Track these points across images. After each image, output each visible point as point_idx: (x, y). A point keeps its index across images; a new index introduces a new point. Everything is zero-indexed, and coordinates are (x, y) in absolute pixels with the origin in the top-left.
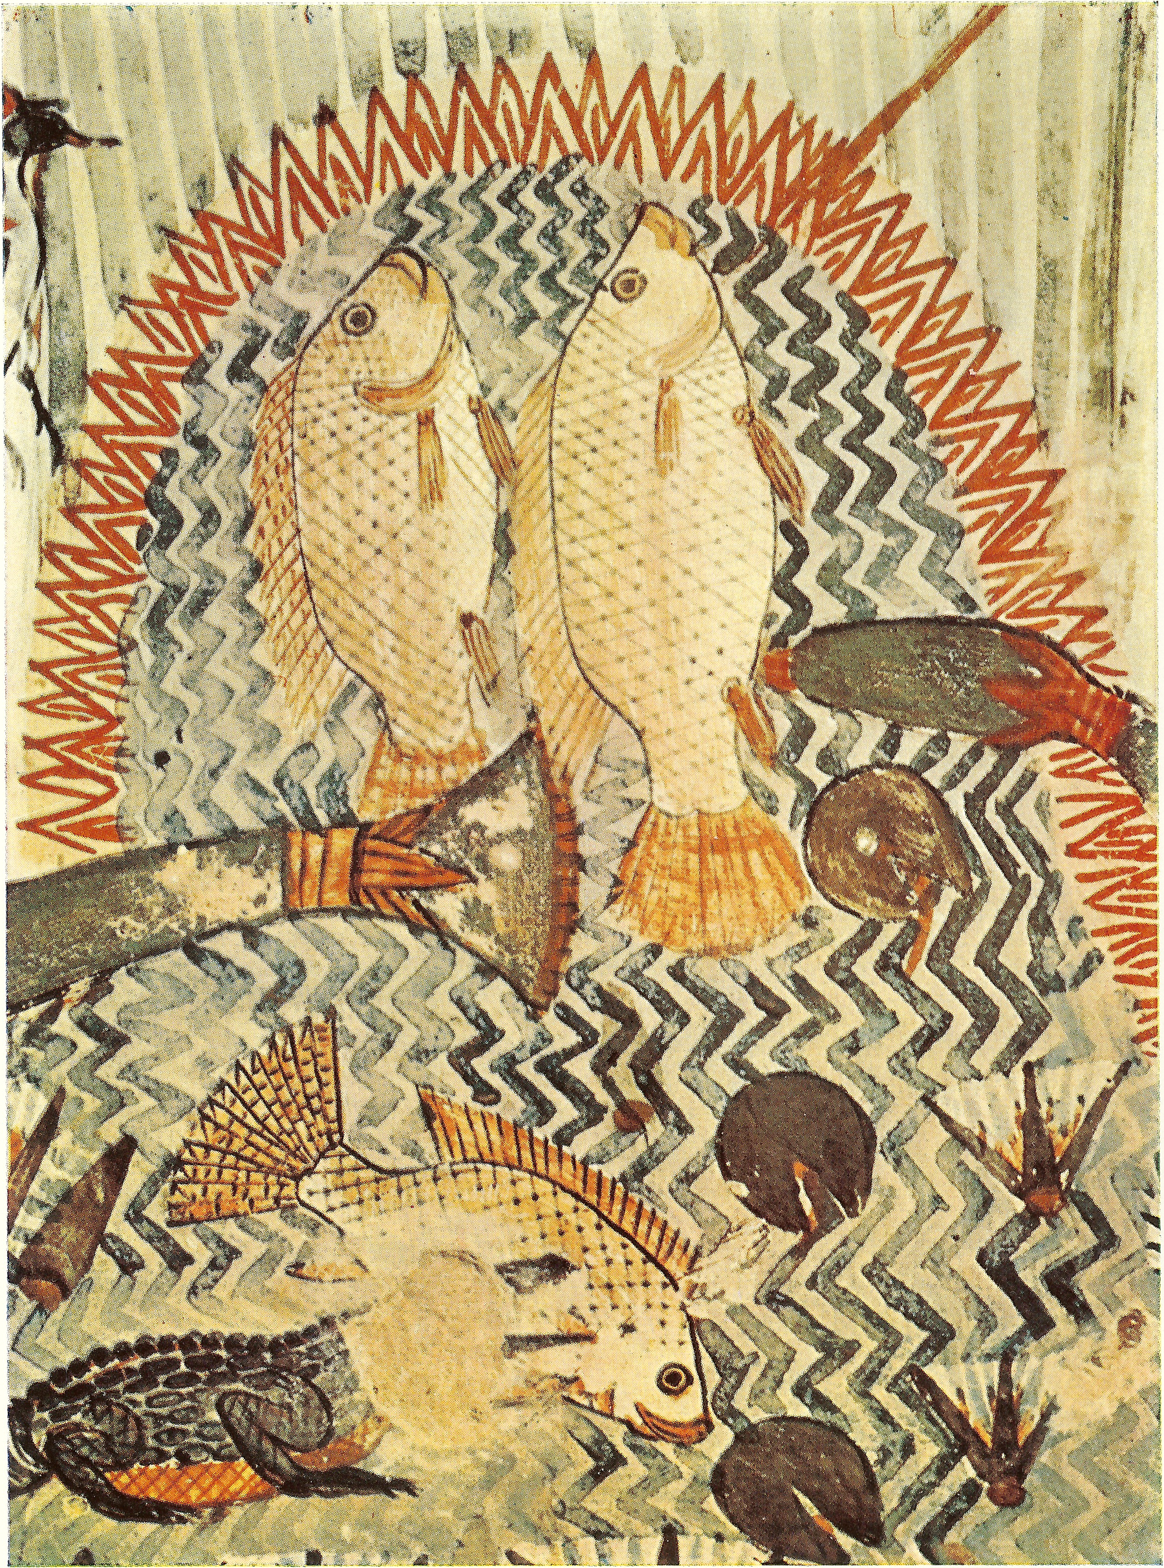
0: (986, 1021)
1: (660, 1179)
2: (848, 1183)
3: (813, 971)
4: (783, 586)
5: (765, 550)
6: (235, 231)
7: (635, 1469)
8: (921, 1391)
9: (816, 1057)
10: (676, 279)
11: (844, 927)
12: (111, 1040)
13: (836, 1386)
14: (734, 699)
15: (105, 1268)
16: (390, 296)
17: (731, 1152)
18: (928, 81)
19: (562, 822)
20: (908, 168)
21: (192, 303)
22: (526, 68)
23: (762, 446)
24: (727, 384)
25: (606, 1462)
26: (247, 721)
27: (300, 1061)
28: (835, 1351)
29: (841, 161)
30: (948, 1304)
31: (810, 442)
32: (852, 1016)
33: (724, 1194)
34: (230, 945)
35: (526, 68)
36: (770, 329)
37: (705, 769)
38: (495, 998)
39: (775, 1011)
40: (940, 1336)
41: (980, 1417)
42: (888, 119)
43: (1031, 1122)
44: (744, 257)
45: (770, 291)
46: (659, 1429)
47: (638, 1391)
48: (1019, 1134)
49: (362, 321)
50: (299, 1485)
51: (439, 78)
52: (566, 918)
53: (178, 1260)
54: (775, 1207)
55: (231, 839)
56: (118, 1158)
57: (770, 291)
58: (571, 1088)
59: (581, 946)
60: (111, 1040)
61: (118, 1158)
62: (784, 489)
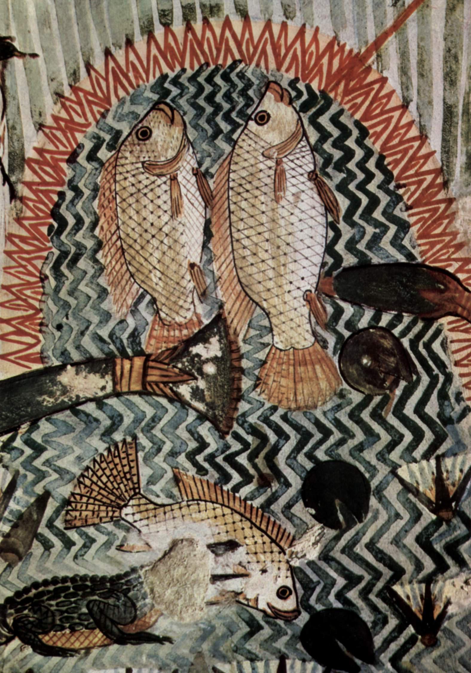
0: (418, 436)
1: (277, 507)
2: (358, 510)
3: (343, 417)
4: (330, 249)
7: (267, 631)
9: (344, 452)
11: (356, 397)
12: (39, 449)
14: (307, 298)
15: (37, 548)
17: (307, 495)
23: (321, 189)
28: (353, 580)
31: (342, 188)
34: (90, 408)
36: (324, 135)
39: (326, 433)
40: (398, 573)
44: (313, 105)
45: (324, 120)
46: (277, 613)
49: (145, 134)
50: (122, 639)
53: (68, 544)
54: (325, 517)
56: (42, 501)
57: (324, 120)
61: (42, 501)
62: (330, 207)
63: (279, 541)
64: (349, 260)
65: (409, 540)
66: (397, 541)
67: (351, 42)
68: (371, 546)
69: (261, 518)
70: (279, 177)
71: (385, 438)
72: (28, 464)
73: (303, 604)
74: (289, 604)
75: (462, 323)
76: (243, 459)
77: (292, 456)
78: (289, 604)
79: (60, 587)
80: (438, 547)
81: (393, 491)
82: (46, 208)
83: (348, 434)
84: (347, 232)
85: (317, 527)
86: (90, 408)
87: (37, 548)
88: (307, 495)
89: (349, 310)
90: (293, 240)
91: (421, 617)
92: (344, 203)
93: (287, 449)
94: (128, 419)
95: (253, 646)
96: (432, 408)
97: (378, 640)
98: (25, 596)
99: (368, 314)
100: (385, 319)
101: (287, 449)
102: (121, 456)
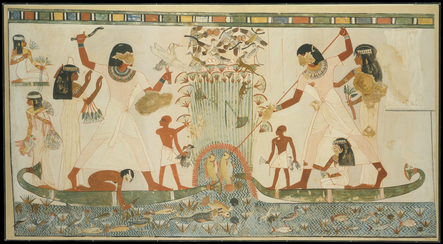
0: (245, 195)
1: (227, 204)
2: (237, 204)
3: (235, 192)
4: (233, 171)
5: (232, 170)
6: (203, 153)
7: (226, 219)
8: (241, 214)
9: (235, 197)
10: (228, 156)
11: (237, 190)
12: (197, 197)
13: (236, 215)
14: (231, 178)
15: (197, 209)
16: (212, 156)
17: (231, 202)
18: (247, 137)
19: (221, 185)
20: (240, 149)
21: (201, 157)
22: (219, 144)
23: (232, 164)
24: (230, 161)
25: (224, 219)
26: (203, 180)
27: (207, 197)
28: (236, 213)
29: (236, 148)
30: (242, 210)
31: (235, 164)
32: (237, 195)
33: (230, 204)
34: (204, 192)
35: (219, 144)
36: (232, 157)
37: (229, 182)
38: (218, 194)
39: (233, 195)
40: (242, 212)
41: (244, 216)
42: (239, 146)
43: (247, 200)
44: (231, 154)
45: (232, 156)
46: (227, 217)
47: (226, 215)
48: (413, 168)
49: (210, 157)
50: (208, 220)
51: (214, 144)
52: (222, 190)
53: (201, 208)
54: (233, 205)
55: (203, 186)
56: (197, 203)
57: (232, 156)
58: (221, 199)
59: (222, 192)
60: (197, 197)
61: (197, 203)
62: (233, 166)
63: (228, 208)
64: (236, 173)
65: (244, 208)
66: (242, 208)
67: (236, 146)
68: (239, 209)
69: (225, 205)
70: (227, 163)
71: (240, 195)
72: (196, 199)
73: (230, 216)
74: (228, 216)
75: (238, 143)
76: (223, 198)
77: (229, 198)
78: (228, 216)
79: (200, 214)
80: (247, 209)
81: (241, 201)
82: (198, 167)
83: (236, 195)
84: (235, 169)
85: (232, 206)
86: (204, 192)
87: (197, 209)
88: (231, 202)
89: (236, 179)
90: (228, 171)
91: (162, 127)
92: (235, 166)
93: (228, 197)
94: (208, 193)
95: (224, 221)
96: (246, 191)
97: (240, 220)
98: (111, 182)
99: (238, 179)
100: (240, 180)
101: (228, 197)
102: (207, 197)
